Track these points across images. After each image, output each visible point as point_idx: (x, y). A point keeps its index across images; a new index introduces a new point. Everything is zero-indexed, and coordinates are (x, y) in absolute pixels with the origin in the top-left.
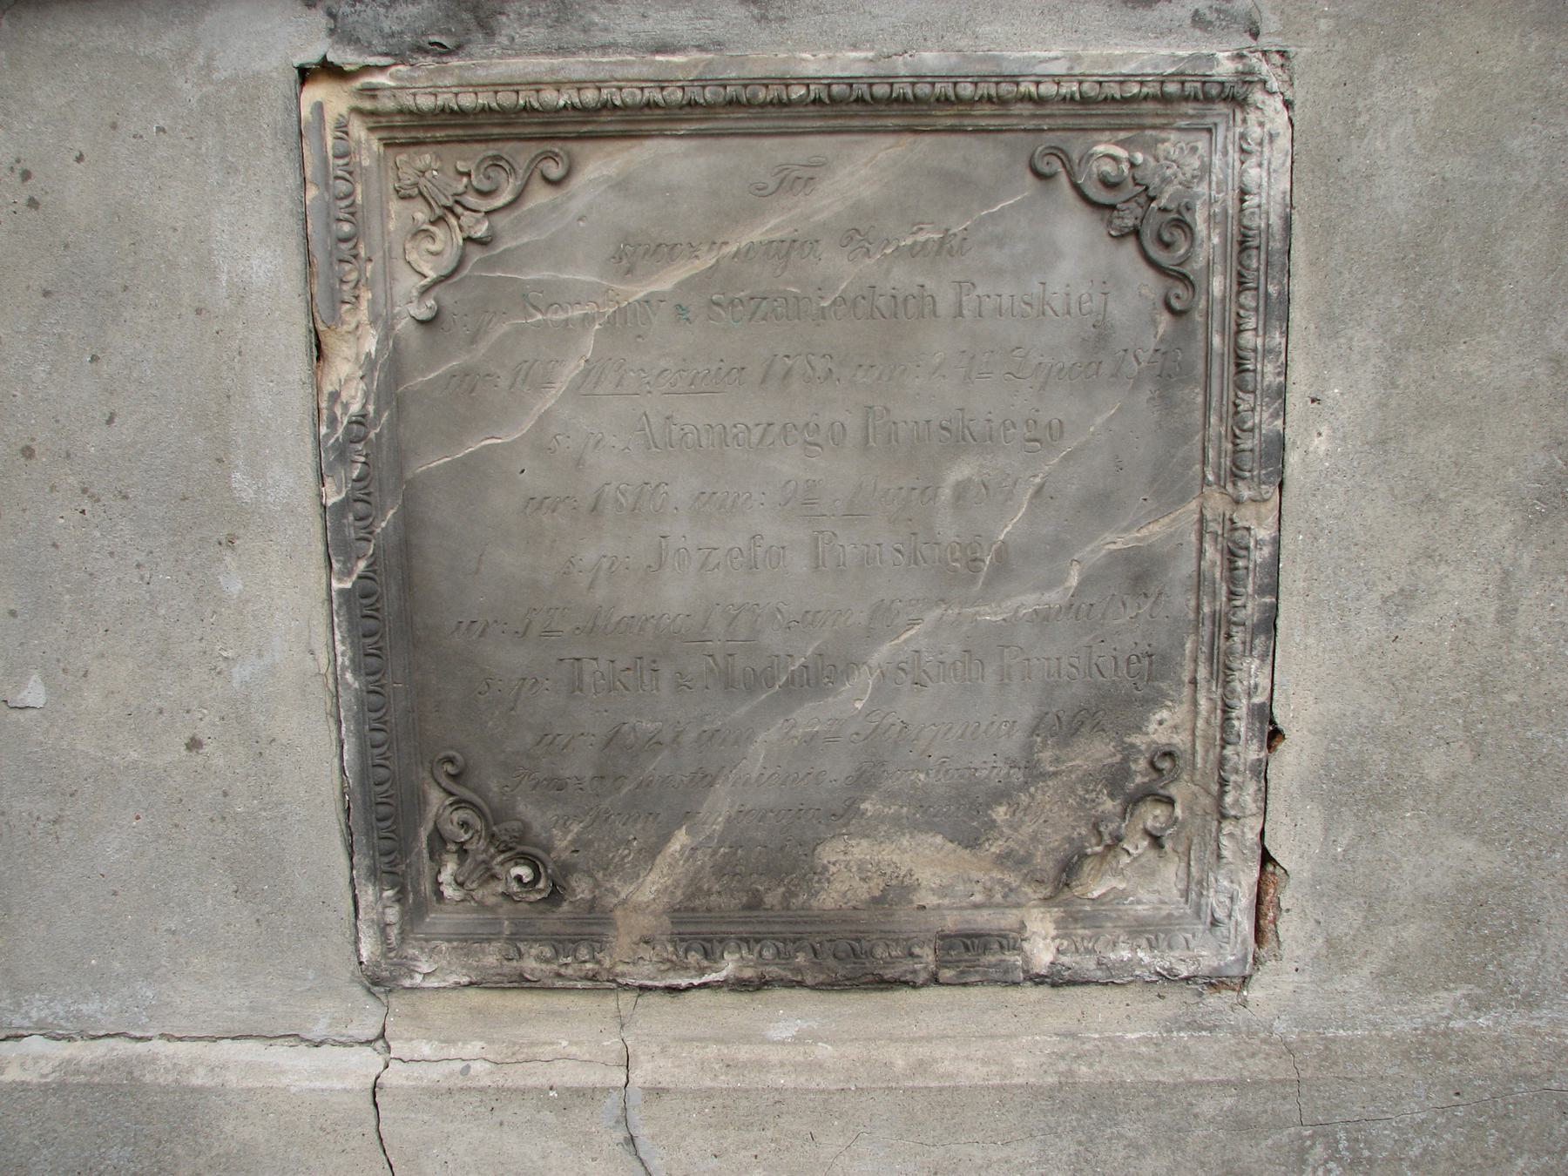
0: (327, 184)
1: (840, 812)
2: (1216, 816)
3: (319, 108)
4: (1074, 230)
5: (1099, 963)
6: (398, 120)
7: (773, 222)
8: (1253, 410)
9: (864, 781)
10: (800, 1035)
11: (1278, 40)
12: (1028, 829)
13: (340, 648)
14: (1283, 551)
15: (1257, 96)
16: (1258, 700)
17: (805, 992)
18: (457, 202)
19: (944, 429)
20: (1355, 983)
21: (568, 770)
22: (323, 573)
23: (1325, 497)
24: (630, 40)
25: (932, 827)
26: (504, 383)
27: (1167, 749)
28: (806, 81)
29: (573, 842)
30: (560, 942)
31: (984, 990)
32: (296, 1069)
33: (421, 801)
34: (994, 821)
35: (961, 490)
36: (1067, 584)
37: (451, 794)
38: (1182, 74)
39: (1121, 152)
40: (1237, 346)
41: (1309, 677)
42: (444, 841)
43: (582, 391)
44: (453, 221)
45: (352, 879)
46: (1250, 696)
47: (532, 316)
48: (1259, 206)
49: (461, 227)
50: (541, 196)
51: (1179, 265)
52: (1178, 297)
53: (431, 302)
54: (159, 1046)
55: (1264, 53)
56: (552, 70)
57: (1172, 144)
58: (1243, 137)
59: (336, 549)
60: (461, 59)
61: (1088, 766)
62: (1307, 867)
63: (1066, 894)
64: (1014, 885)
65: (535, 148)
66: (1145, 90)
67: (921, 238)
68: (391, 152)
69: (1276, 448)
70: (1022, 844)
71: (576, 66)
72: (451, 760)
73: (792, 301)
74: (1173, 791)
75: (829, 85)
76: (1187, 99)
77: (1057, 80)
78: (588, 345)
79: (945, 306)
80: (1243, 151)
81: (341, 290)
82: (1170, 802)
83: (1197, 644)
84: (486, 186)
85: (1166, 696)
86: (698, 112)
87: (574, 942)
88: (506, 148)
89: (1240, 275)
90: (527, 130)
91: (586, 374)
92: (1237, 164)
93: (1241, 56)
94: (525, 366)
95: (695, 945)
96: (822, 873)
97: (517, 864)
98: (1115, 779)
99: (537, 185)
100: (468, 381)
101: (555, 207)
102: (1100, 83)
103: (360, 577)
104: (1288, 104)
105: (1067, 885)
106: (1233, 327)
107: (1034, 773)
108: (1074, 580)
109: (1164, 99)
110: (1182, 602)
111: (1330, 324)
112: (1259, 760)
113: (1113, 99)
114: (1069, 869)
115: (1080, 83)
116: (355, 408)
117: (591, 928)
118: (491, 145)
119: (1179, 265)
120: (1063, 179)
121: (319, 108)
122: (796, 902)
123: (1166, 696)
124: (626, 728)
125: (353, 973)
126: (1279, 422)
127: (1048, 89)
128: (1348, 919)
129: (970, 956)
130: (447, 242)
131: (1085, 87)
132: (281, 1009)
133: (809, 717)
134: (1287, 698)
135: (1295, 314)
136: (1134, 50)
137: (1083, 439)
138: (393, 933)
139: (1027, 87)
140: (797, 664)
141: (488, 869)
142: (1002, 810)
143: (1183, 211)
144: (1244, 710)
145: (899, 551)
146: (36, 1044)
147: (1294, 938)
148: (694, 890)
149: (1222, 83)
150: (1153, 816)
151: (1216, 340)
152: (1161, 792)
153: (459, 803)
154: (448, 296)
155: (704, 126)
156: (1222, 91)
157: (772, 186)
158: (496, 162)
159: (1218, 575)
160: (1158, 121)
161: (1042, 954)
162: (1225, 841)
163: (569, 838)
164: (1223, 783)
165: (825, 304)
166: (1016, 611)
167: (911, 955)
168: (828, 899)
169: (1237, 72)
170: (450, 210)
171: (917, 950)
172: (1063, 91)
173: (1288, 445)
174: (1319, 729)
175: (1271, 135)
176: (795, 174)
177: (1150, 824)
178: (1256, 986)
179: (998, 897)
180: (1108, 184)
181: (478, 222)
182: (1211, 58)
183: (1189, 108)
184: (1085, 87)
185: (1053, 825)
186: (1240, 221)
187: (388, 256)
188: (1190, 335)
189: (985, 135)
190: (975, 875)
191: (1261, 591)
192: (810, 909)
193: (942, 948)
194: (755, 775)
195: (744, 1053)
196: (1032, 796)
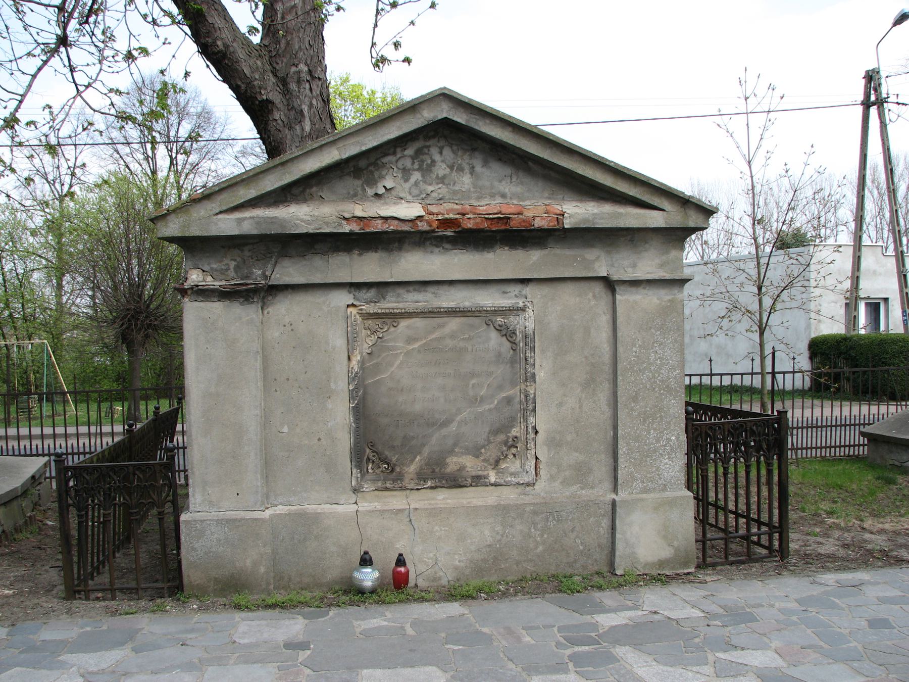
4: (494, 335)
9: (455, 444)
10: (444, 498)
20: (557, 484)
25: (469, 454)
32: (339, 509)
33: (365, 451)
35: (473, 385)
41: (542, 420)
50: (392, 329)
57: (512, 318)
69: (534, 375)
71: (401, 305)
79: (470, 348)
88: (386, 320)
98: (506, 443)
107: (489, 442)
111: (543, 351)
114: (497, 462)
117: (400, 477)
128: (554, 470)
129: (478, 481)
130: (374, 338)
133: (444, 431)
146: (280, 507)
150: (514, 450)
161: (493, 479)
168: (448, 470)
180: (500, 326)
195: (433, 502)
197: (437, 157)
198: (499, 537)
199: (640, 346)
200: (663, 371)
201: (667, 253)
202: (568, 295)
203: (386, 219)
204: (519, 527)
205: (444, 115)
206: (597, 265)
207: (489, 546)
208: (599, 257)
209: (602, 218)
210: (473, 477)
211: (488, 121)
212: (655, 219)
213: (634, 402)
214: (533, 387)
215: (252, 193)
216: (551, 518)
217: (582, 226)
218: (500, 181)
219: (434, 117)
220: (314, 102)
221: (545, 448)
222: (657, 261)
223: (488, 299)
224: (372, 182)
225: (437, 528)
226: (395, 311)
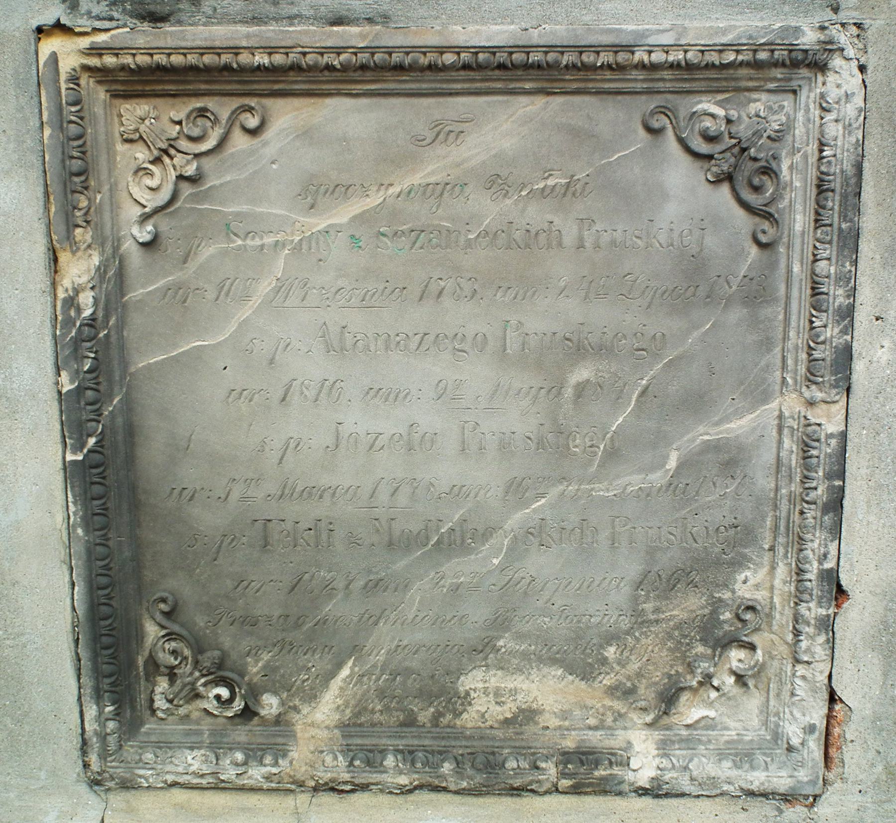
0: (61, 127)
1: (480, 648)
2: (790, 661)
3: (54, 59)
4: (680, 176)
5: (692, 779)
6: (122, 76)
7: (430, 168)
8: (825, 326)
9: (500, 624)
11: (855, 14)
12: (634, 666)
13: (72, 508)
14: (849, 443)
15: (837, 62)
16: (829, 565)
17: (449, 796)
18: (171, 146)
19: (567, 339)
21: (260, 610)
22: (60, 447)
23: (886, 398)
24: (312, 12)
25: (554, 661)
26: (211, 295)
27: (750, 603)
28: (458, 50)
29: (264, 667)
30: (252, 750)
31: (596, 798)
33: (140, 636)
34: (606, 659)
35: (581, 389)
36: (667, 467)
37: (163, 627)
38: (772, 44)
39: (721, 112)
40: (813, 273)
42: (157, 665)
43: (274, 304)
44: (166, 160)
45: (80, 698)
46: (820, 563)
47: (234, 242)
48: (835, 156)
49: (174, 166)
50: (240, 142)
51: (765, 205)
52: (764, 232)
53: (150, 228)
55: (843, 25)
56: (248, 36)
57: (759, 104)
58: (822, 96)
59: (74, 428)
60: (172, 25)
61: (684, 616)
62: (869, 706)
63: (666, 720)
64: (623, 711)
65: (236, 102)
66: (740, 58)
67: (551, 182)
68: (117, 102)
69: (845, 358)
70: (629, 678)
71: (271, 32)
72: (164, 600)
73: (444, 233)
74: (755, 639)
75: (477, 53)
76: (776, 64)
77: (666, 49)
78: (279, 266)
79: (569, 238)
80: (823, 109)
81: (73, 216)
82: (752, 647)
83: (777, 519)
84: (196, 132)
85: (750, 560)
86: (369, 75)
87: (263, 750)
88: (210, 103)
89: (817, 213)
90: (228, 87)
91: (278, 290)
92: (817, 119)
93: (823, 28)
94: (228, 283)
95: (360, 755)
96: (465, 698)
97: (217, 685)
99: (237, 134)
100: (179, 296)
101: (252, 152)
102: (702, 52)
103: (89, 451)
104: (862, 68)
105: (665, 713)
106: (811, 258)
107: (641, 621)
108: (672, 463)
109: (757, 65)
110: (764, 482)
112: (828, 616)
113: (713, 65)
114: (669, 698)
115: (686, 52)
116: (87, 313)
117: (277, 737)
118: (201, 99)
119: (765, 205)
120: (670, 133)
121: (54, 59)
122: (444, 721)
123: (750, 560)
124: (307, 576)
125: (78, 775)
126: (849, 338)
127: (658, 57)
130: (163, 178)
131: (690, 55)
132: (17, 804)
133: (459, 569)
134: (851, 565)
135: (863, 246)
136: (733, 23)
137: (681, 349)
138: (112, 740)
139: (640, 55)
140: (446, 528)
141: (194, 689)
142: (612, 649)
143: (771, 161)
144: (815, 571)
145: (529, 438)
147: (859, 766)
149: (806, 51)
150: (736, 657)
151: (796, 268)
152: (744, 638)
153: (170, 636)
154: (164, 223)
155: (373, 87)
156: (806, 58)
157: (430, 136)
158: (202, 112)
159: (794, 463)
160: (751, 84)
161: (644, 766)
162: (798, 681)
163: (260, 665)
164: (797, 633)
165: (471, 236)
166: (625, 489)
167: (537, 768)
168: (469, 719)
169: (820, 42)
170: (165, 152)
171: (543, 765)
172: (671, 58)
173: (855, 356)
174: (878, 591)
175: (847, 95)
176: (448, 128)
177: (735, 664)
178: (825, 804)
179: (609, 720)
180: (710, 139)
181: (188, 162)
182: (797, 29)
183: (778, 73)
184: (690, 55)
185: (654, 664)
186: (819, 168)
187: (113, 189)
188: (773, 266)
189: (605, 96)
190: (589, 703)
191: (829, 476)
192: (454, 727)
193: (561, 762)
194: (411, 617)
196: (638, 640)
210: (566, 757)
214: (838, 409)
221: (873, 663)
226: (245, 58)
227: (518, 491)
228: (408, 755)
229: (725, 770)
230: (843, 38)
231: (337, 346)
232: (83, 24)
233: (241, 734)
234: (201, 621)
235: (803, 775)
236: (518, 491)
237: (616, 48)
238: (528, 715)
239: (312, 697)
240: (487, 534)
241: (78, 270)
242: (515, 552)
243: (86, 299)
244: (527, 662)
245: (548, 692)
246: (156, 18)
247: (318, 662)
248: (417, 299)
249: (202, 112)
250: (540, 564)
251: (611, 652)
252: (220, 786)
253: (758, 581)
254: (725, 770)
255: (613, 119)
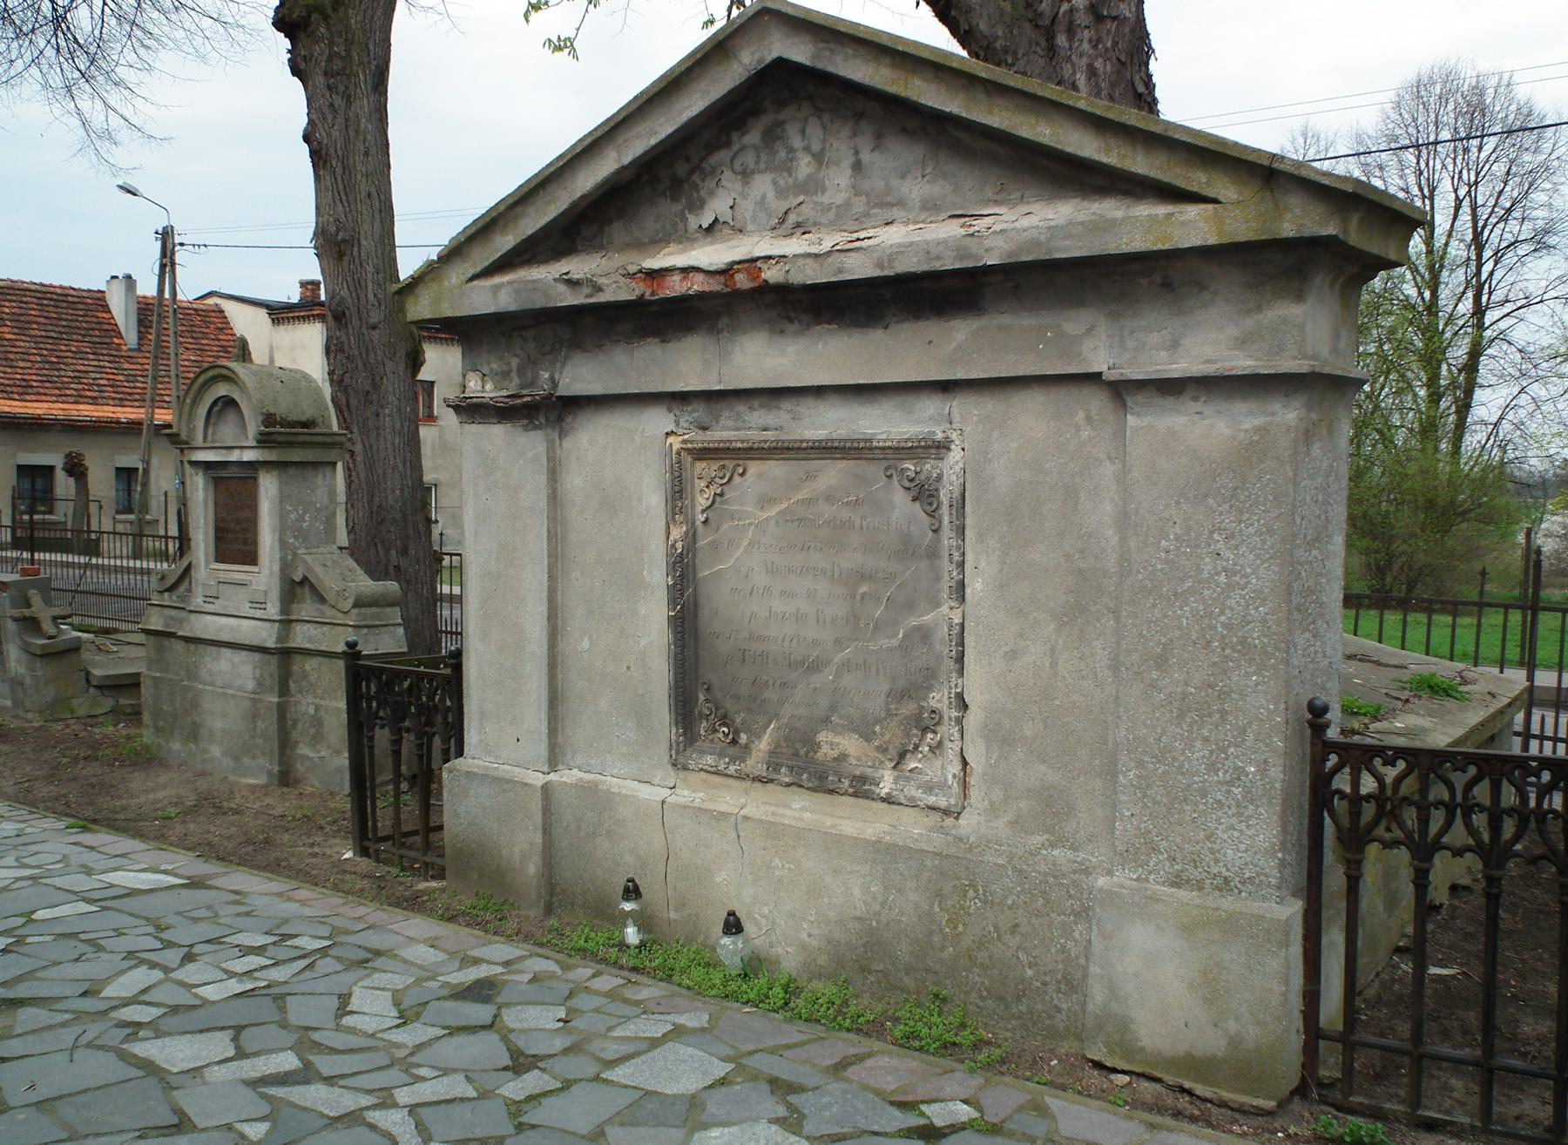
4: (900, 499)
9: (833, 708)
10: (799, 809)
12: (887, 737)
20: (1001, 825)
25: (854, 731)
32: (645, 792)
33: (697, 700)
35: (863, 596)
41: (977, 683)
54: (609, 778)
59: (672, 602)
79: (857, 526)
88: (726, 462)
98: (918, 719)
100: (715, 545)
107: (889, 714)
111: (981, 537)
114: (902, 756)
128: (997, 794)
129: (861, 788)
130: (709, 493)
133: (817, 680)
146: (575, 771)
148: (778, 746)
154: (710, 514)
161: (886, 787)
168: (820, 756)
195: (781, 811)
197: (797, 142)
198: (877, 907)
199: (1177, 538)
200: (1231, 602)
201: (1259, 308)
202: (1031, 415)
203: (687, 271)
204: (913, 896)
205: (775, 55)
206: (1086, 347)
207: (860, 919)
208: (1092, 328)
209: (1068, 237)
211: (850, 52)
212: (1191, 227)
213: (1158, 667)
215: (505, 242)
216: (971, 893)
217: (1024, 258)
218: (903, 177)
219: (759, 61)
220: (1098, 64)
222: (1232, 331)
223: (883, 423)
224: (697, 206)
225: (777, 861)
227: (839, 644)
228: (791, 769)
229: (918, 794)
230: (954, 436)
231: (771, 570)
232: (680, 431)
233: (731, 751)
234: (719, 695)
235: (953, 801)
236: (839, 644)
237: (866, 441)
238: (843, 757)
239: (760, 737)
240: (827, 664)
241: (677, 533)
242: (838, 675)
243: (679, 545)
244: (840, 730)
245: (851, 745)
246: (704, 429)
247: (762, 720)
248: (1351, 650)
249: (724, 467)
250: (848, 681)
251: (878, 728)
252: (718, 773)
253: (939, 699)
254: (918, 794)
255: (874, 470)
